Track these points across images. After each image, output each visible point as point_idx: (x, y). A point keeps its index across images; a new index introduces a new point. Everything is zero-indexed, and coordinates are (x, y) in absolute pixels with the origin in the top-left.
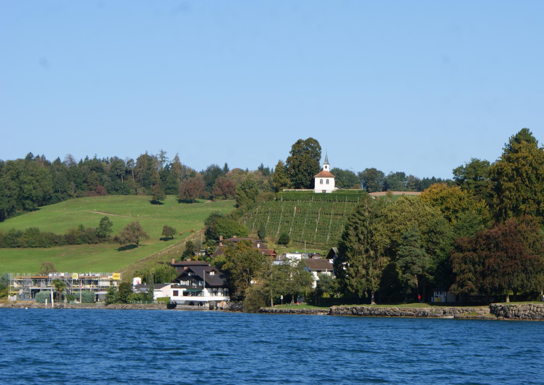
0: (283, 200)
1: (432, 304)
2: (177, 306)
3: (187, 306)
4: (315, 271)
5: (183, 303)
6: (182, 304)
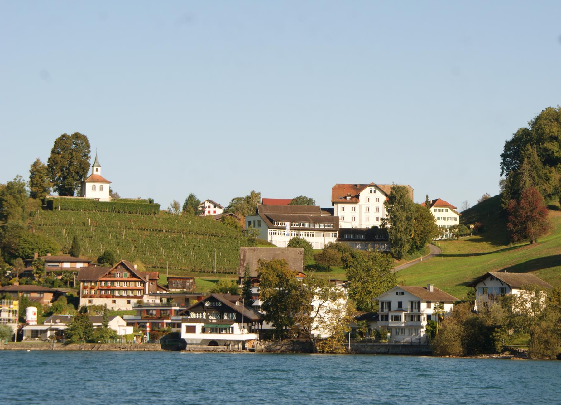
0: (61, 209)
1: (56, 329)
2: (188, 346)
3: (205, 347)
4: (424, 302)
5: (199, 342)
6: (197, 344)
